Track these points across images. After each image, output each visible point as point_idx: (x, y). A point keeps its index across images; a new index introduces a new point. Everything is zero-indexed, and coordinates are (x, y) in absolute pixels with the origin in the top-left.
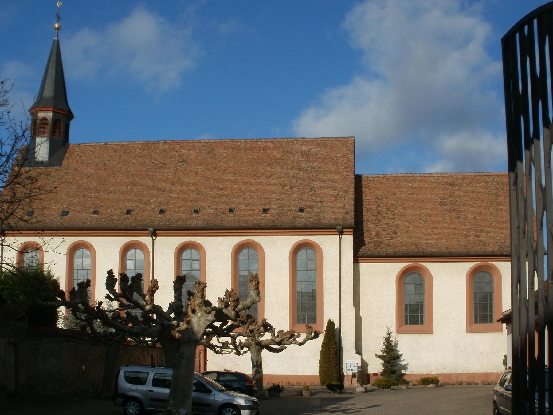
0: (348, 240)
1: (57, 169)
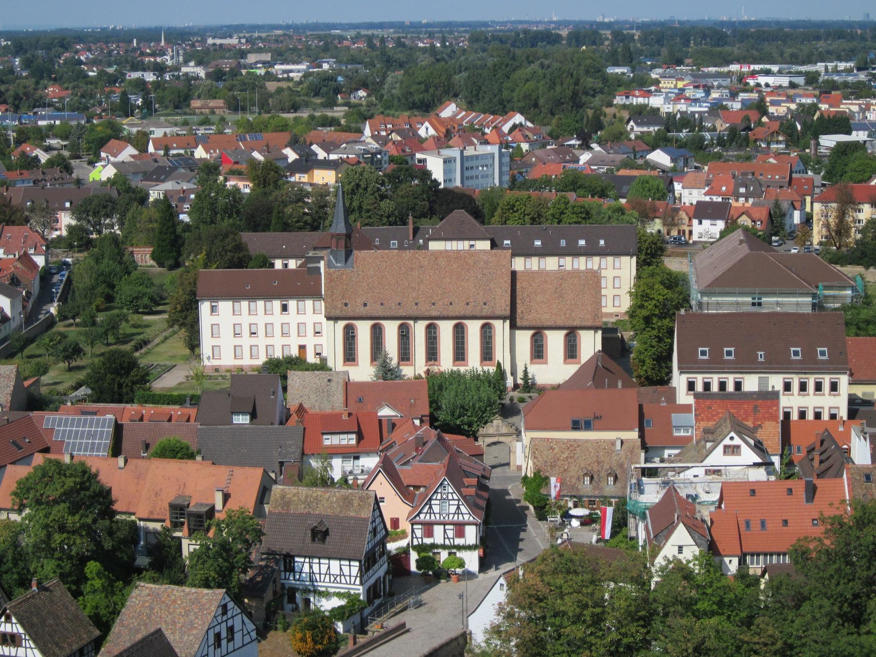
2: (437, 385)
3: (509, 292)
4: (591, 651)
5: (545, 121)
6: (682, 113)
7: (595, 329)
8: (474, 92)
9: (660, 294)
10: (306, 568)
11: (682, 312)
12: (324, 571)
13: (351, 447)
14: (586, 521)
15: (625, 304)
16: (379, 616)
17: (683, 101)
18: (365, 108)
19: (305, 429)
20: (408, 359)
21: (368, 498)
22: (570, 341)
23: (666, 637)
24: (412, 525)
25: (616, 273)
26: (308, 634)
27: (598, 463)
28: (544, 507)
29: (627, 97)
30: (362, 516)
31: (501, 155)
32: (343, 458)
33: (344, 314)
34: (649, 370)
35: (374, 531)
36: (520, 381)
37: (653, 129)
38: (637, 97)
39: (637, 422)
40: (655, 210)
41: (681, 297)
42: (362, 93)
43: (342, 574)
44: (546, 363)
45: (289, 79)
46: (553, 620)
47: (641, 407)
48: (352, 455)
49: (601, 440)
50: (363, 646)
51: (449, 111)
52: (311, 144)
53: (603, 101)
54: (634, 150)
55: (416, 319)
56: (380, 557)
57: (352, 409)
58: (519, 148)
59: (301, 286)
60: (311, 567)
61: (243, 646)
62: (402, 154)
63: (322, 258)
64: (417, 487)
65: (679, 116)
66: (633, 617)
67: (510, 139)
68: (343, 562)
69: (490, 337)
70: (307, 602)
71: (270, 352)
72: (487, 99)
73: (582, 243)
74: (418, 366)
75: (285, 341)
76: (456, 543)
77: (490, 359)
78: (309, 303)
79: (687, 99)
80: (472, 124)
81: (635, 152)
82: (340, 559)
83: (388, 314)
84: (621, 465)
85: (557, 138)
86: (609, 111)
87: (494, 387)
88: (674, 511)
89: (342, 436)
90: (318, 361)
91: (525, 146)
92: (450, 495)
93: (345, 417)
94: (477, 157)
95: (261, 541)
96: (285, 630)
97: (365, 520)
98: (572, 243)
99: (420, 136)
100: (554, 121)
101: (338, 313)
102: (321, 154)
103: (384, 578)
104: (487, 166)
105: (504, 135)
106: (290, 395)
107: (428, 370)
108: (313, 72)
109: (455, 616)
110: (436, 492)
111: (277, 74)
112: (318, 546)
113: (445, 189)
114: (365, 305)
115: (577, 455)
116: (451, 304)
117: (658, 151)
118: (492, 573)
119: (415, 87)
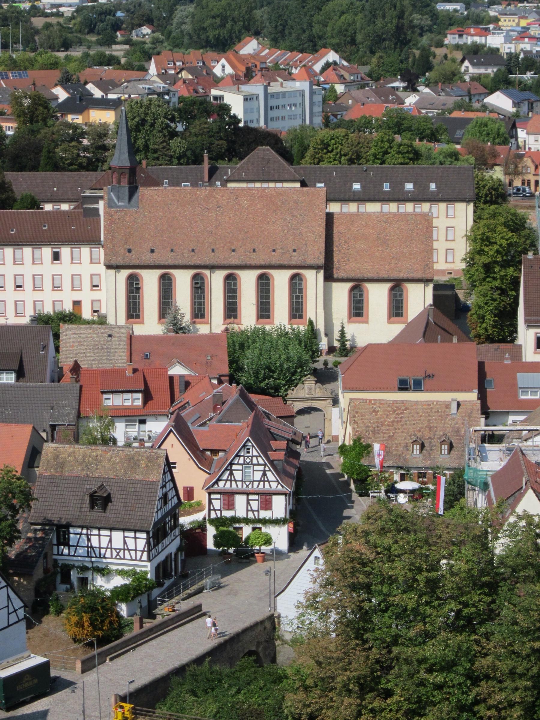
0: (321, 274)
2: (238, 346)
3: (323, 236)
4: (425, 624)
5: (364, 60)
6: (525, 52)
7: (426, 281)
8: (280, 28)
9: (502, 238)
10: (84, 541)
11: (530, 255)
12: (104, 544)
13: (137, 408)
14: (415, 495)
15: (462, 248)
16: (171, 597)
17: (526, 40)
18: (150, 45)
19: (81, 387)
20: (203, 316)
21: (157, 458)
22: (395, 296)
23: (515, 606)
24: (210, 494)
25: (450, 222)
26: (86, 618)
27: (430, 429)
28: (366, 480)
29: (461, 36)
30: (151, 479)
31: (312, 93)
32: (127, 421)
33: (127, 262)
34: (489, 328)
35: (165, 498)
36: (336, 344)
37: (491, 71)
38: (472, 35)
39: (476, 382)
40: (495, 155)
41: (528, 242)
42: (146, 30)
43: (126, 549)
44: (367, 322)
45: (59, 15)
46: (379, 587)
47: (481, 365)
48: (138, 418)
49: (433, 402)
50: (151, 631)
51: (250, 47)
52: (86, 83)
53: (432, 40)
54: (469, 92)
55: (213, 268)
56: (171, 531)
57: (139, 364)
58: (333, 90)
59: (78, 232)
60: (89, 540)
61: (9, 626)
62: (195, 95)
63: (101, 198)
64: (215, 452)
65: (522, 56)
66: (476, 584)
67: (322, 79)
68: (127, 534)
69: (301, 291)
70: (84, 581)
71: (39, 307)
72: (294, 36)
73: (409, 186)
74: (216, 323)
75: (57, 295)
76: (261, 517)
77: (301, 317)
78: (85, 251)
79: (531, 38)
80: (276, 65)
81: (470, 95)
82: (124, 530)
83: (181, 262)
84: (457, 432)
85: (377, 80)
86: (439, 52)
87: (306, 346)
88: (522, 475)
89: (126, 396)
90: (96, 318)
91: (340, 88)
92: (254, 459)
93: (129, 373)
94: (284, 94)
95: (29, 506)
96: (58, 613)
97: (154, 483)
98: (397, 186)
99: (215, 75)
100: (374, 60)
101: (120, 261)
102: (98, 93)
103: (176, 554)
104: (295, 105)
105: (316, 75)
106: (61, 356)
107: (227, 330)
108: (87, 6)
109: (260, 599)
110: (237, 455)
111: (44, 9)
112: (97, 514)
113: (246, 127)
114: (152, 251)
115: (404, 420)
116: (254, 250)
117: (498, 93)
118: (304, 552)
119: (209, 21)
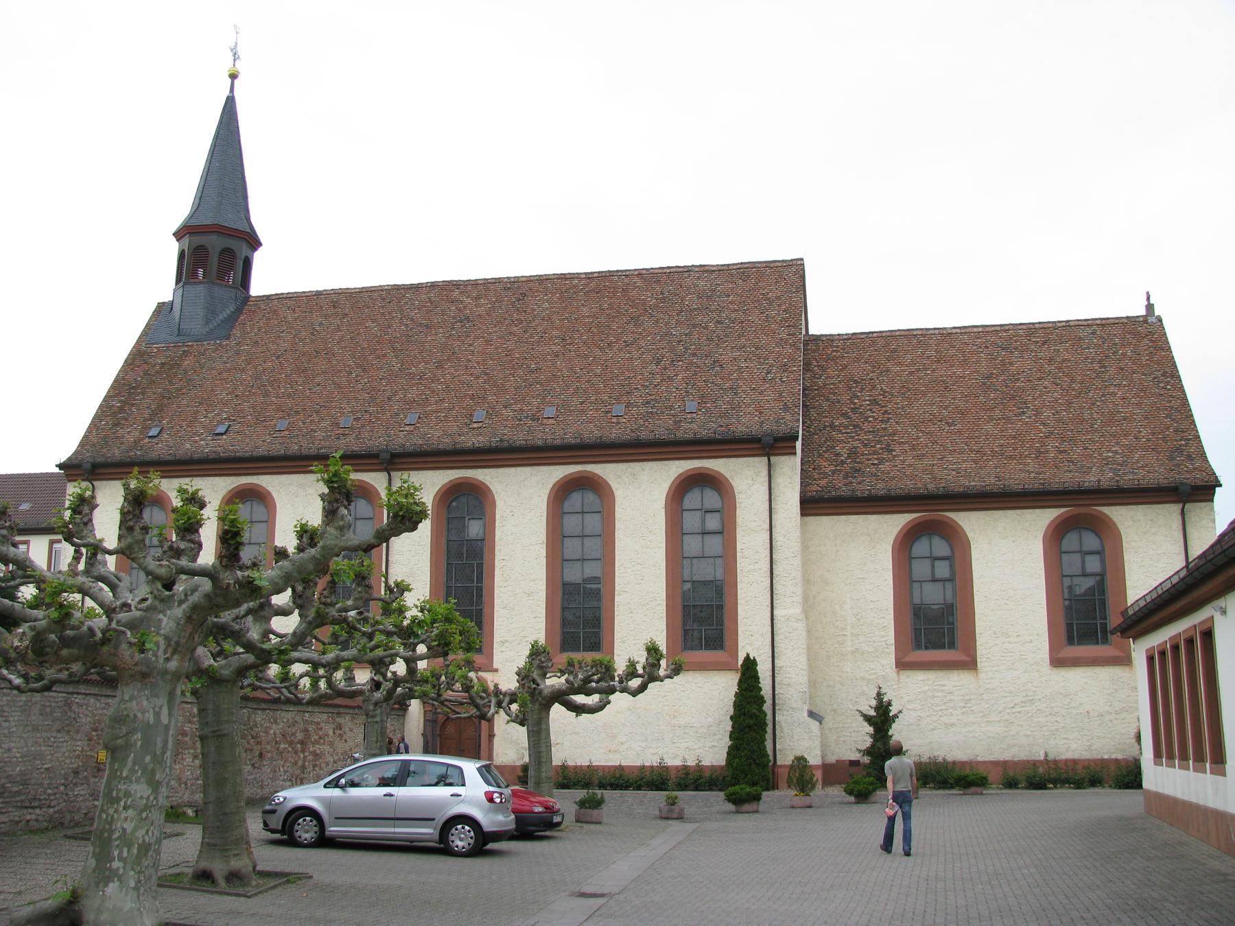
1: (220, 345)
44: (969, 663)
